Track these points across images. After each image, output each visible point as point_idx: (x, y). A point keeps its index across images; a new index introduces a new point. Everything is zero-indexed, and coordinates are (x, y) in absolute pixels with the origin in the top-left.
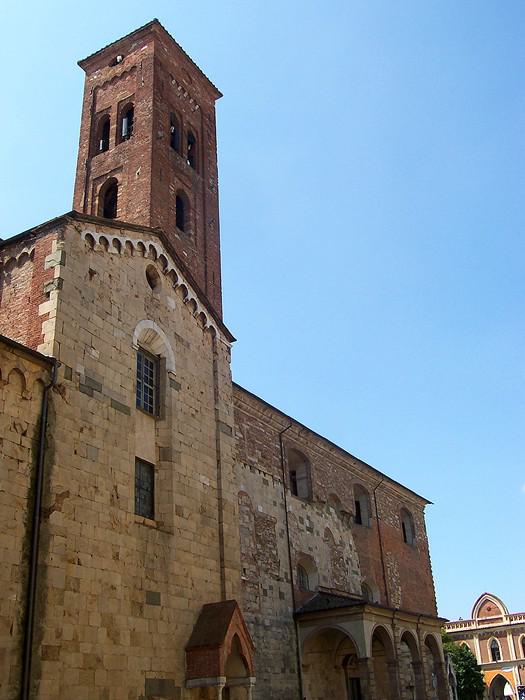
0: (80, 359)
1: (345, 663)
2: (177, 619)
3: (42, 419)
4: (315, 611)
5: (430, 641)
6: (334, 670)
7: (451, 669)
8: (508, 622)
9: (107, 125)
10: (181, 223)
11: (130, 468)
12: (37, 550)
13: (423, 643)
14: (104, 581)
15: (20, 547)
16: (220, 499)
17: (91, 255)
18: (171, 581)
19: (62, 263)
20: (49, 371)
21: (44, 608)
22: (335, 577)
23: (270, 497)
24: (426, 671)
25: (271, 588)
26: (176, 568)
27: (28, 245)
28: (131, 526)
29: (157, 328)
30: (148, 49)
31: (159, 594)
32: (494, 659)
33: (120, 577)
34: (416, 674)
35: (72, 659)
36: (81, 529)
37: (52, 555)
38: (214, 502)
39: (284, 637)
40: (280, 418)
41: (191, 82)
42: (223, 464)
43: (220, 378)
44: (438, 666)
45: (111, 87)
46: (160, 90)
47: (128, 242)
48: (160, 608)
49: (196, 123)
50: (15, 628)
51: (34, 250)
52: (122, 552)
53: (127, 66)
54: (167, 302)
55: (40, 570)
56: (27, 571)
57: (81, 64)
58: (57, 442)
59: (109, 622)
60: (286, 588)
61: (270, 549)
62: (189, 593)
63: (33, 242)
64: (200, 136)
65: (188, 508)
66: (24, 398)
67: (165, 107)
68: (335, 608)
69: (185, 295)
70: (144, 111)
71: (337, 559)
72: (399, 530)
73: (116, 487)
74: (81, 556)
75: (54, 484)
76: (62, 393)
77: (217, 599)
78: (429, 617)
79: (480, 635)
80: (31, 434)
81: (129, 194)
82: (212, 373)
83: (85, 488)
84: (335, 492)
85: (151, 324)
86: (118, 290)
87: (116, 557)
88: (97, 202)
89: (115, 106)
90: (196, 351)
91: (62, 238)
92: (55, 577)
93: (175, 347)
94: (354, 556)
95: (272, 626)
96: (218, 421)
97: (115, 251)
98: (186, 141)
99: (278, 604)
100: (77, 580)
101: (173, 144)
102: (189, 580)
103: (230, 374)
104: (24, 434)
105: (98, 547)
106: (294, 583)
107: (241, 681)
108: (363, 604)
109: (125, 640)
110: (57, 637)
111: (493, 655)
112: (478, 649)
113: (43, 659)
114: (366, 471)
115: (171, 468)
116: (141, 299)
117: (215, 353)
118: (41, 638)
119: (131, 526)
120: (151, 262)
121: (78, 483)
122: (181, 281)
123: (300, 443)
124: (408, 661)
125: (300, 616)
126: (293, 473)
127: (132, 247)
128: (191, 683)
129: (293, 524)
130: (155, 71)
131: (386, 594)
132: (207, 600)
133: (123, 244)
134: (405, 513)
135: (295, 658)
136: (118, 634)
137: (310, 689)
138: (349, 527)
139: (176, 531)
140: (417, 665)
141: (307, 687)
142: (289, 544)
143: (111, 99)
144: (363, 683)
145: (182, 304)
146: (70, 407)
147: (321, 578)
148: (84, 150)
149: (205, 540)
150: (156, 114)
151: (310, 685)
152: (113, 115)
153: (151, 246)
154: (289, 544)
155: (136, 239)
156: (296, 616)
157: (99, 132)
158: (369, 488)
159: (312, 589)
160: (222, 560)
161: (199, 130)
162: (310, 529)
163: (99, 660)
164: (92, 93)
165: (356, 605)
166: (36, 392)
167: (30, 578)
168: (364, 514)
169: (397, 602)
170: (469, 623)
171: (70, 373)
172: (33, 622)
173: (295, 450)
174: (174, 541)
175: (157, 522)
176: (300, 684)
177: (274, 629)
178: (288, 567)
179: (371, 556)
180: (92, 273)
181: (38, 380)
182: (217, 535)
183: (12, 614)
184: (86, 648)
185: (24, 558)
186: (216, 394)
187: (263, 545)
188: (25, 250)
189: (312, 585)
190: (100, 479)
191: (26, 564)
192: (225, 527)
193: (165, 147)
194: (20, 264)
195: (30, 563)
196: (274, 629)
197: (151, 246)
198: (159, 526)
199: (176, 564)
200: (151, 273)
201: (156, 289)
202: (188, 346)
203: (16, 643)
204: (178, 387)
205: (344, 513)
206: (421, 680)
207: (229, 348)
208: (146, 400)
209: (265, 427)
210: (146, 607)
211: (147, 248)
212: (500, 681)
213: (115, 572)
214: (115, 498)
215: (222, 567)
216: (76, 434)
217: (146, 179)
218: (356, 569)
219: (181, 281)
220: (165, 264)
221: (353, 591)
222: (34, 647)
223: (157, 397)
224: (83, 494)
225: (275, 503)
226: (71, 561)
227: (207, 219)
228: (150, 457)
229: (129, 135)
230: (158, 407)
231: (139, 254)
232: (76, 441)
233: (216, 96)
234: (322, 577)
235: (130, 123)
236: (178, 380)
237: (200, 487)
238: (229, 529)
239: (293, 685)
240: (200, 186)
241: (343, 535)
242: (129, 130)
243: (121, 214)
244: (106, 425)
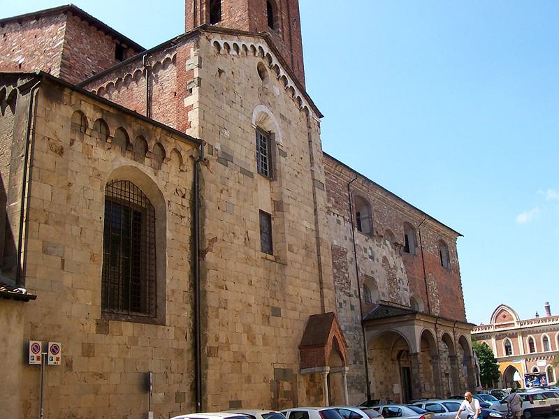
0: (217, 139)
1: (399, 357)
2: (291, 328)
5: (463, 341)
7: (476, 361)
8: (519, 327)
10: (271, 22)
11: (256, 217)
12: (199, 280)
13: (457, 342)
14: (244, 300)
15: (187, 279)
16: (317, 238)
17: (219, 58)
18: (287, 299)
19: (200, 66)
21: (207, 320)
22: (391, 293)
23: (342, 233)
24: (459, 362)
25: (345, 302)
26: (290, 290)
27: (170, 51)
28: (259, 260)
29: (268, 111)
31: (280, 309)
32: (507, 354)
33: (253, 298)
34: (452, 364)
35: (226, 355)
36: (226, 264)
37: (209, 284)
38: (314, 240)
39: (354, 338)
40: (348, 173)
42: (319, 212)
44: (468, 359)
48: (281, 318)
52: (254, 280)
54: (273, 89)
55: (201, 294)
58: (207, 201)
60: (355, 301)
61: (344, 273)
62: (300, 307)
63: (173, 50)
65: (295, 245)
66: (182, 171)
69: (286, 84)
71: (392, 279)
72: (438, 257)
73: (247, 232)
74: (227, 283)
75: (207, 232)
76: (207, 165)
77: (319, 312)
78: (462, 323)
79: (496, 336)
80: (188, 197)
82: (307, 143)
83: (227, 234)
85: (264, 108)
86: (239, 84)
87: (250, 283)
88: (204, 8)
90: (296, 126)
91: (197, 46)
92: (212, 299)
93: (281, 125)
94: (404, 277)
95: (346, 330)
96: (313, 179)
97: (235, 53)
99: (350, 313)
100: (226, 300)
102: (300, 299)
103: (321, 146)
104: (183, 197)
105: (238, 277)
106: (362, 298)
107: (339, 369)
108: (414, 313)
109: (259, 342)
110: (216, 341)
111: (507, 350)
112: (495, 346)
113: (208, 356)
114: (413, 211)
115: (283, 217)
118: (206, 342)
119: (259, 260)
120: (260, 59)
121: (222, 231)
122: (282, 73)
123: (363, 190)
124: (445, 355)
126: (358, 214)
128: (304, 371)
129: (360, 253)
131: (428, 306)
132: (312, 312)
133: (240, 47)
134: (442, 243)
135: (363, 353)
137: (374, 376)
138: (401, 255)
139: (289, 263)
140: (453, 358)
141: (372, 374)
142: (357, 269)
145: (284, 91)
146: (214, 174)
147: (381, 294)
149: (308, 269)
151: (374, 373)
153: (260, 47)
154: (357, 269)
156: (363, 322)
158: (415, 224)
160: (321, 283)
162: (372, 257)
163: (243, 356)
165: (410, 314)
166: (189, 165)
167: (195, 301)
168: (411, 245)
170: (488, 327)
172: (200, 330)
173: (359, 196)
174: (289, 271)
175: (275, 257)
177: (347, 332)
178: (357, 286)
179: (417, 277)
180: (220, 72)
181: (174, 149)
182: (317, 265)
183: (186, 326)
184: (235, 347)
186: (312, 158)
187: (338, 270)
188: (168, 56)
189: (374, 299)
190: (236, 227)
192: (322, 258)
194: (164, 67)
196: (347, 332)
198: (277, 259)
201: (265, 80)
202: (290, 123)
203: (190, 346)
204: (285, 155)
205: (396, 244)
206: (456, 369)
207: (319, 123)
209: (337, 179)
210: (271, 318)
211: (257, 49)
212: (511, 370)
213: (250, 294)
215: (321, 288)
216: (218, 194)
219: (282, 73)
220: (270, 61)
222: (202, 347)
223: (270, 163)
225: (346, 238)
226: (221, 287)
227: (291, 19)
228: (268, 209)
231: (252, 54)
232: (219, 200)
234: (381, 293)
236: (284, 149)
237: (303, 229)
238: (325, 261)
239: (361, 373)
241: (396, 261)
244: (238, 187)
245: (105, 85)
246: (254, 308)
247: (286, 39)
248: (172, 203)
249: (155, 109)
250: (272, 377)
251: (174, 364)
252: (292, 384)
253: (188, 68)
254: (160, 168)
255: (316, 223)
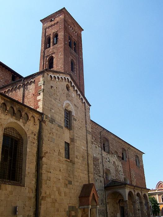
1: (119, 202)
3: (39, 131)
4: (111, 186)
5: (145, 196)
6: (116, 204)
9: (49, 39)
10: (72, 69)
11: (63, 144)
14: (57, 177)
15: (34, 168)
16: (87, 153)
17: (51, 82)
18: (75, 178)
19: (44, 84)
20: (41, 116)
21: (42, 185)
23: (98, 152)
25: (98, 179)
26: (76, 174)
27: (32, 78)
29: (69, 103)
30: (62, 17)
33: (61, 176)
34: (140, 205)
35: (49, 200)
41: (74, 26)
42: (88, 143)
43: (87, 117)
44: (147, 203)
45: (50, 28)
46: (66, 29)
47: (64, 78)
49: (76, 39)
50: (34, 192)
51: (35, 80)
53: (55, 22)
56: (37, 175)
57: (41, 21)
58: (44, 137)
59: (59, 190)
60: (102, 179)
62: (80, 181)
63: (34, 78)
64: (77, 43)
66: (35, 125)
67: (67, 34)
68: (117, 185)
69: (77, 92)
70: (61, 35)
71: (117, 170)
73: (60, 150)
75: (43, 149)
76: (45, 123)
77: (87, 183)
78: (145, 188)
80: (37, 135)
81: (57, 61)
84: (116, 150)
85: (68, 102)
86: (59, 92)
87: (60, 171)
88: (47, 63)
89: (52, 34)
91: (43, 77)
93: (74, 108)
95: (98, 190)
96: (87, 130)
97: (58, 80)
98: (73, 44)
99: (100, 183)
101: (70, 46)
104: (35, 135)
105: (55, 168)
108: (125, 184)
109: (63, 195)
110: (45, 194)
116: (65, 94)
117: (85, 110)
118: (41, 194)
120: (67, 83)
122: (76, 88)
123: (106, 135)
125: (107, 188)
126: (104, 144)
127: (62, 79)
129: (104, 160)
130: (64, 23)
132: (85, 183)
133: (60, 78)
134: (137, 157)
135: (105, 200)
136: (61, 193)
139: (76, 163)
140: (141, 203)
141: (108, 209)
143: (51, 32)
144: (125, 208)
146: (47, 126)
148: (43, 47)
149: (83, 165)
150: (65, 36)
152: (52, 37)
153: (67, 78)
155: (63, 76)
156: (105, 187)
157: (47, 42)
158: (126, 149)
159: (109, 179)
160: (88, 171)
161: (77, 41)
162: (109, 161)
163: (56, 201)
164: (45, 30)
165: (123, 185)
166: (37, 123)
168: (125, 157)
169: (134, 183)
170: (155, 190)
171: (47, 117)
173: (104, 137)
174: (76, 166)
176: (106, 208)
177: (99, 191)
180: (52, 87)
182: (87, 164)
183: (33, 187)
185: (36, 171)
186: (86, 122)
188: (32, 80)
191: (36, 173)
193: (67, 46)
194: (30, 84)
195: (38, 172)
197: (67, 78)
199: (76, 173)
200: (67, 86)
202: (78, 108)
203: (34, 195)
205: (119, 156)
208: (68, 124)
214: (59, 153)
215: (88, 174)
216: (49, 135)
217: (62, 57)
218: (122, 173)
219: (76, 88)
220: (71, 84)
221: (121, 180)
224: (51, 152)
228: (68, 141)
229: (56, 43)
230: (70, 126)
232: (49, 137)
233: (82, 30)
234: (112, 176)
235: (57, 39)
236: (75, 118)
239: (104, 208)
240: (78, 58)
241: (119, 163)
242: (57, 41)
243: (55, 68)
244: (56, 132)
245: (7, 90)
246: (61, 181)
247: (78, 76)
248: (30, 137)
249: (26, 100)
250: (67, 210)
251: (27, 203)
252: (75, 212)
253: (39, 85)
254: (26, 123)
255: (87, 147)
